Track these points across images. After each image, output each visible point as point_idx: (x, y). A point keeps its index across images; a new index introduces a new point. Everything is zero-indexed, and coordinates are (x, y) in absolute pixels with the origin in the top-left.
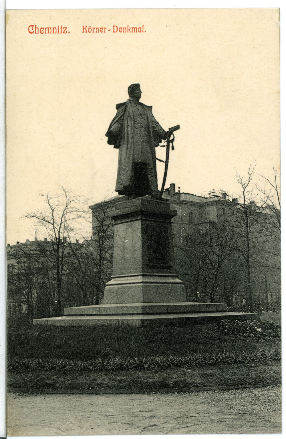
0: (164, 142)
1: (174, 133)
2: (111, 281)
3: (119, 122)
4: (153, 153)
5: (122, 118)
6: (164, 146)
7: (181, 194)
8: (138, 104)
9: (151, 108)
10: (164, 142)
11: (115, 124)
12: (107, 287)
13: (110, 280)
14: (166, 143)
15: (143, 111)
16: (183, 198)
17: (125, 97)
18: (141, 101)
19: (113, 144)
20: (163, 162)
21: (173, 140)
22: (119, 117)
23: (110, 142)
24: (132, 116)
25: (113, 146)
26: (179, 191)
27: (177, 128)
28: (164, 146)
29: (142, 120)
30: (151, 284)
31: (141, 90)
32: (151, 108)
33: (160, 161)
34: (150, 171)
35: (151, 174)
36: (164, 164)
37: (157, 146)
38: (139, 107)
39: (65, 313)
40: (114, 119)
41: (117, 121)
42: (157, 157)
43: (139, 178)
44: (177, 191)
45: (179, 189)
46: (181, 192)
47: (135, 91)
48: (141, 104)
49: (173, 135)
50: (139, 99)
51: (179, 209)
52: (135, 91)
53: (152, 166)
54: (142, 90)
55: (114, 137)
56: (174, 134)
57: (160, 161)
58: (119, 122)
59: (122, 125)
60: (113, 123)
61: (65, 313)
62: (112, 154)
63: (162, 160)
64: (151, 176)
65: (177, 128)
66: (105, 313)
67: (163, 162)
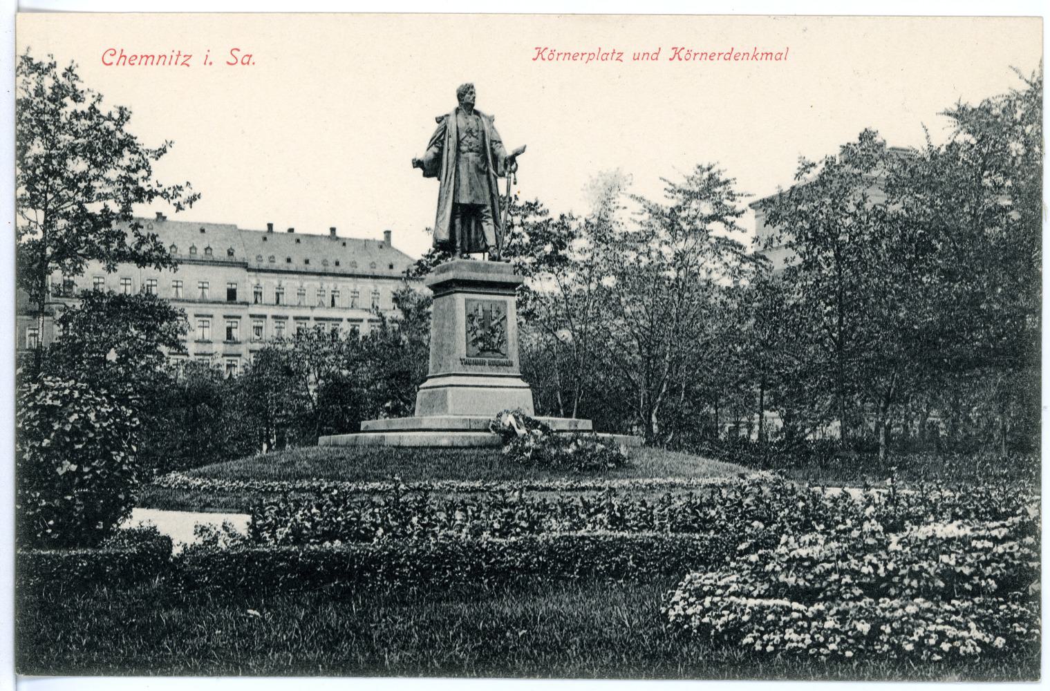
47: (466, 99)
52: (466, 99)
59: (441, 149)
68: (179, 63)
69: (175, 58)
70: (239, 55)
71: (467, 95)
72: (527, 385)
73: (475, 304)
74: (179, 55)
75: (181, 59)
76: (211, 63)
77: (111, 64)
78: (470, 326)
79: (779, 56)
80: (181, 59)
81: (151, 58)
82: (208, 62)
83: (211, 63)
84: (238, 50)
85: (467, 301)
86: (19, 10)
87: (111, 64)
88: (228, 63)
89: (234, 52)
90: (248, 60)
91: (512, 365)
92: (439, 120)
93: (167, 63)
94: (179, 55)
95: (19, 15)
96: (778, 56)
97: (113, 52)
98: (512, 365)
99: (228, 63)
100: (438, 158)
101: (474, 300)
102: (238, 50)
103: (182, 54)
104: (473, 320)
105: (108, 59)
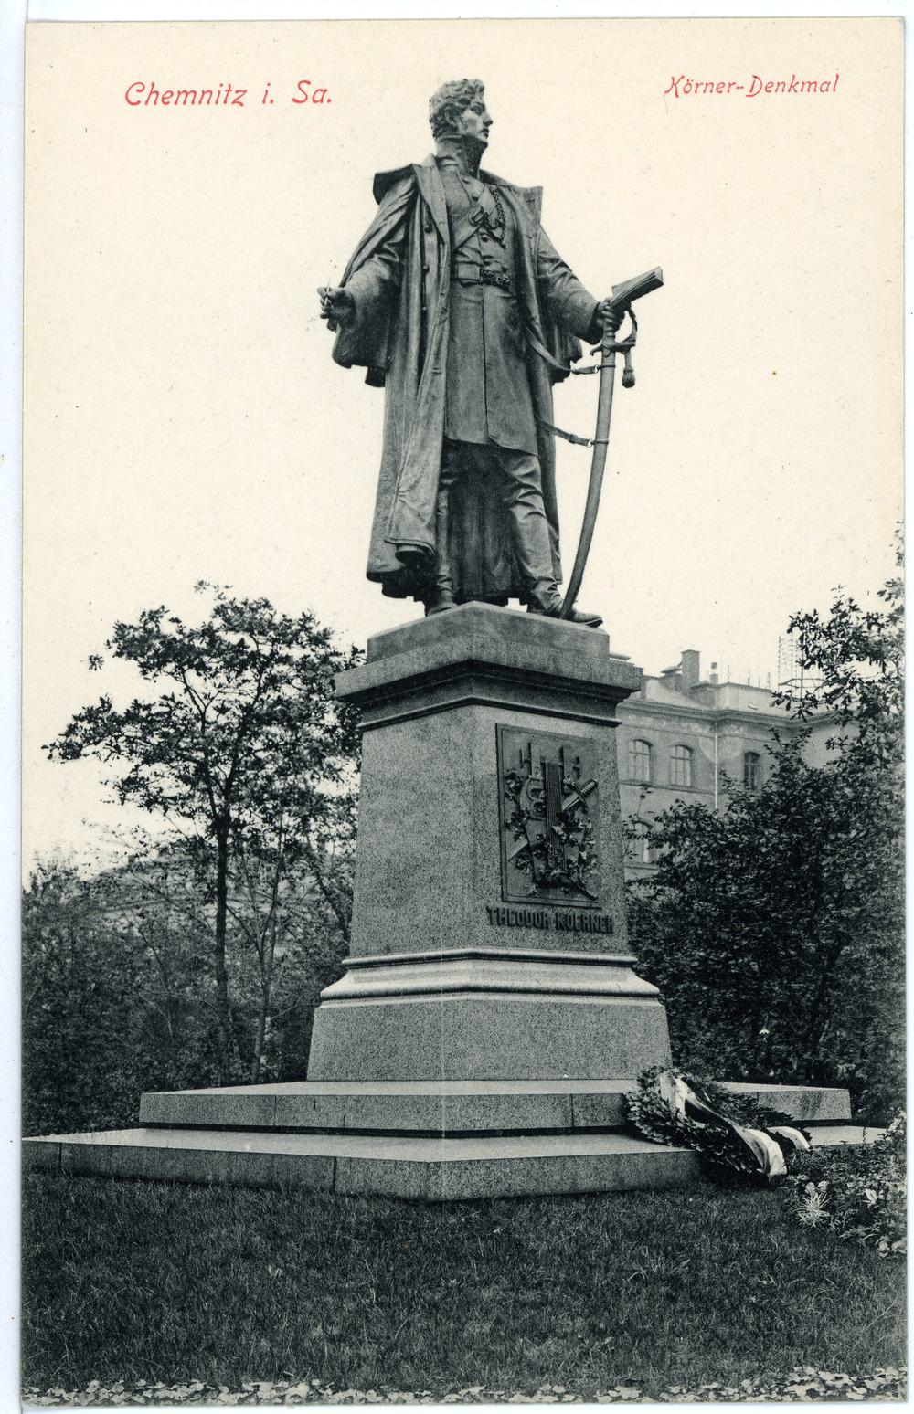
0: (592, 353)
1: (635, 305)
2: (341, 981)
3: (384, 256)
4: (539, 408)
5: (400, 236)
6: (591, 370)
7: (719, 687)
8: (474, 175)
9: (533, 198)
10: (592, 353)
11: (367, 267)
12: (324, 1006)
13: (340, 977)
14: (599, 354)
15: (498, 206)
16: (726, 701)
17: (417, 145)
18: (488, 163)
19: (362, 365)
20: (584, 442)
21: (631, 341)
22: (446, 334)
23: (344, 359)
24: (444, 229)
25: (360, 372)
26: (714, 677)
27: (652, 283)
28: (591, 370)
29: (490, 248)
30: (447, 952)
31: (541, 223)
32: (533, 198)
33: (572, 439)
34: (526, 486)
35: (526, 499)
36: (588, 451)
37: (559, 376)
38: (476, 187)
39: (144, 1116)
40: (364, 245)
41: (379, 249)
42: (560, 421)
43: (476, 525)
44: (704, 676)
45: (712, 672)
46: (722, 681)
47: (459, 120)
48: (487, 179)
49: (632, 316)
50: (480, 153)
51: (713, 739)
52: (459, 120)
53: (535, 465)
54: (492, 111)
55: (366, 330)
56: (636, 312)
57: (572, 439)
58: (384, 256)
59: (399, 270)
60: (359, 260)
61: (144, 1116)
62: (359, 405)
63: (580, 434)
64: (528, 510)
65: (652, 283)
66: (298, 1125)
67: (584, 442)
68: (230, 99)
69: (223, 94)
70: (310, 90)
71: (469, 114)
72: (654, 989)
73: (519, 742)
74: (229, 91)
75: (233, 96)
76: (272, 102)
77: (139, 102)
78: (510, 807)
79: (825, 87)
80: (233, 96)
81: (191, 96)
82: (268, 100)
83: (272, 102)
84: (308, 83)
85: (501, 732)
86: (27, 21)
87: (139, 102)
88: (295, 100)
89: (304, 86)
90: (321, 96)
91: (610, 931)
92: (384, 184)
93: (213, 100)
94: (229, 91)
95: (28, 25)
96: (824, 87)
97: (140, 87)
98: (610, 931)
99: (295, 100)
100: (392, 293)
101: (520, 731)
102: (308, 83)
103: (234, 88)
104: (518, 790)
105: (134, 96)
